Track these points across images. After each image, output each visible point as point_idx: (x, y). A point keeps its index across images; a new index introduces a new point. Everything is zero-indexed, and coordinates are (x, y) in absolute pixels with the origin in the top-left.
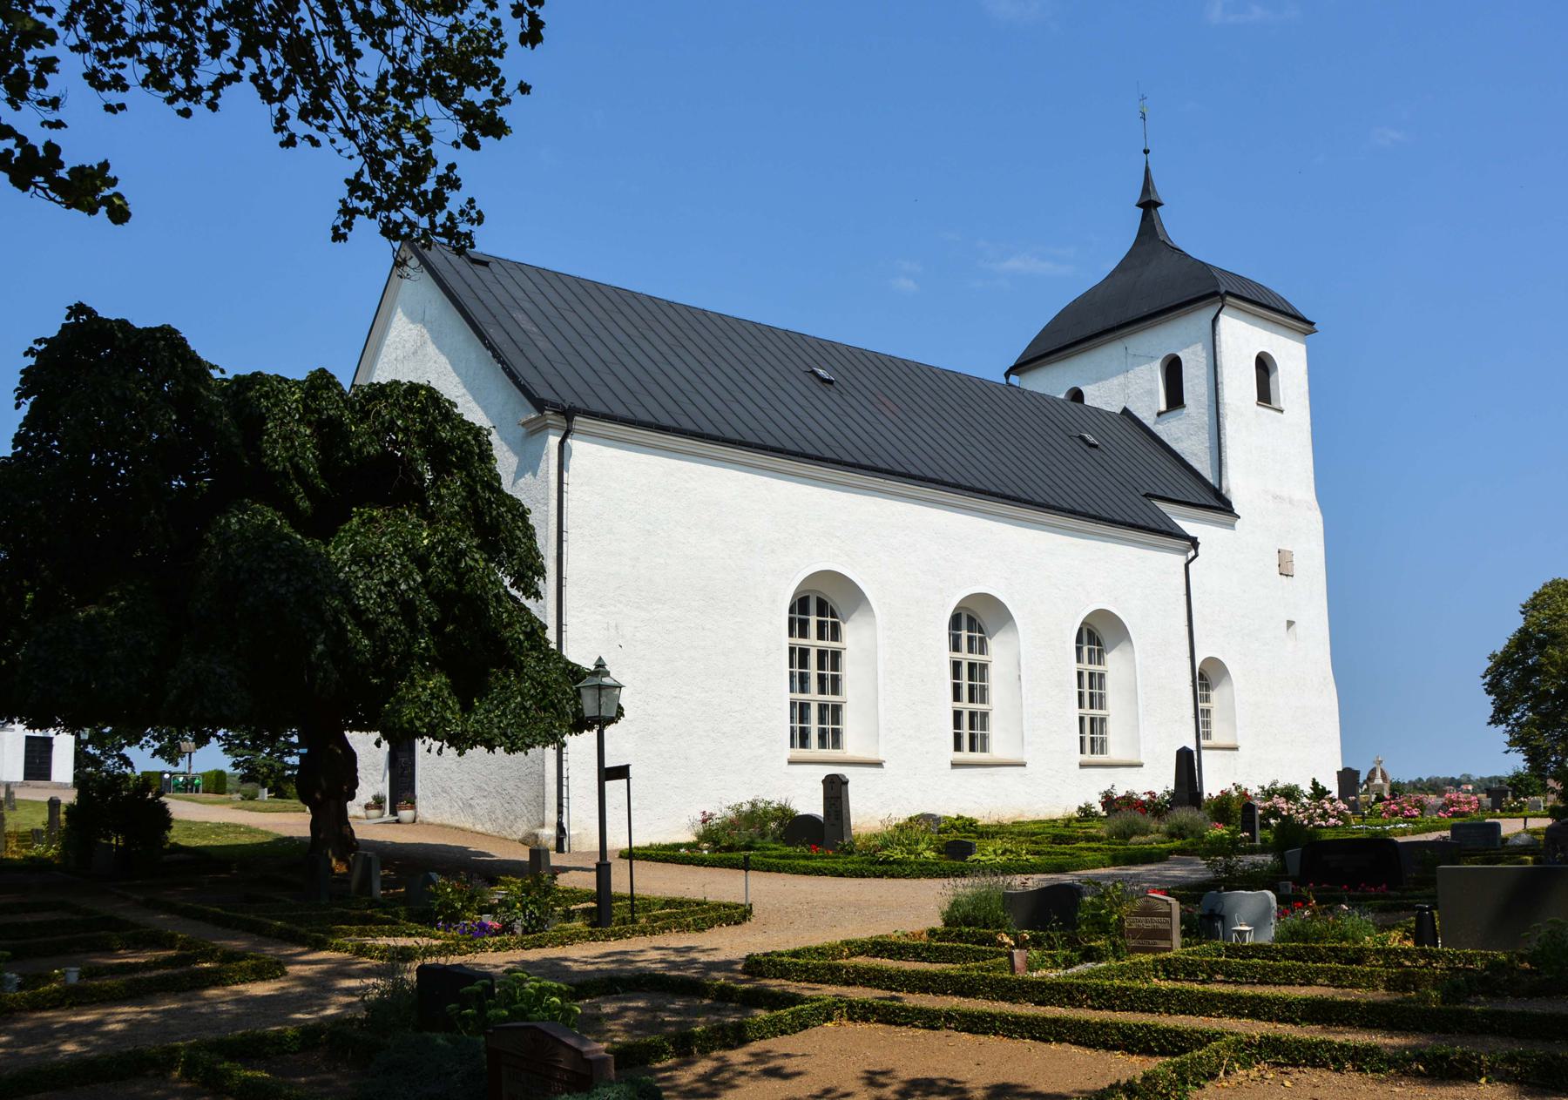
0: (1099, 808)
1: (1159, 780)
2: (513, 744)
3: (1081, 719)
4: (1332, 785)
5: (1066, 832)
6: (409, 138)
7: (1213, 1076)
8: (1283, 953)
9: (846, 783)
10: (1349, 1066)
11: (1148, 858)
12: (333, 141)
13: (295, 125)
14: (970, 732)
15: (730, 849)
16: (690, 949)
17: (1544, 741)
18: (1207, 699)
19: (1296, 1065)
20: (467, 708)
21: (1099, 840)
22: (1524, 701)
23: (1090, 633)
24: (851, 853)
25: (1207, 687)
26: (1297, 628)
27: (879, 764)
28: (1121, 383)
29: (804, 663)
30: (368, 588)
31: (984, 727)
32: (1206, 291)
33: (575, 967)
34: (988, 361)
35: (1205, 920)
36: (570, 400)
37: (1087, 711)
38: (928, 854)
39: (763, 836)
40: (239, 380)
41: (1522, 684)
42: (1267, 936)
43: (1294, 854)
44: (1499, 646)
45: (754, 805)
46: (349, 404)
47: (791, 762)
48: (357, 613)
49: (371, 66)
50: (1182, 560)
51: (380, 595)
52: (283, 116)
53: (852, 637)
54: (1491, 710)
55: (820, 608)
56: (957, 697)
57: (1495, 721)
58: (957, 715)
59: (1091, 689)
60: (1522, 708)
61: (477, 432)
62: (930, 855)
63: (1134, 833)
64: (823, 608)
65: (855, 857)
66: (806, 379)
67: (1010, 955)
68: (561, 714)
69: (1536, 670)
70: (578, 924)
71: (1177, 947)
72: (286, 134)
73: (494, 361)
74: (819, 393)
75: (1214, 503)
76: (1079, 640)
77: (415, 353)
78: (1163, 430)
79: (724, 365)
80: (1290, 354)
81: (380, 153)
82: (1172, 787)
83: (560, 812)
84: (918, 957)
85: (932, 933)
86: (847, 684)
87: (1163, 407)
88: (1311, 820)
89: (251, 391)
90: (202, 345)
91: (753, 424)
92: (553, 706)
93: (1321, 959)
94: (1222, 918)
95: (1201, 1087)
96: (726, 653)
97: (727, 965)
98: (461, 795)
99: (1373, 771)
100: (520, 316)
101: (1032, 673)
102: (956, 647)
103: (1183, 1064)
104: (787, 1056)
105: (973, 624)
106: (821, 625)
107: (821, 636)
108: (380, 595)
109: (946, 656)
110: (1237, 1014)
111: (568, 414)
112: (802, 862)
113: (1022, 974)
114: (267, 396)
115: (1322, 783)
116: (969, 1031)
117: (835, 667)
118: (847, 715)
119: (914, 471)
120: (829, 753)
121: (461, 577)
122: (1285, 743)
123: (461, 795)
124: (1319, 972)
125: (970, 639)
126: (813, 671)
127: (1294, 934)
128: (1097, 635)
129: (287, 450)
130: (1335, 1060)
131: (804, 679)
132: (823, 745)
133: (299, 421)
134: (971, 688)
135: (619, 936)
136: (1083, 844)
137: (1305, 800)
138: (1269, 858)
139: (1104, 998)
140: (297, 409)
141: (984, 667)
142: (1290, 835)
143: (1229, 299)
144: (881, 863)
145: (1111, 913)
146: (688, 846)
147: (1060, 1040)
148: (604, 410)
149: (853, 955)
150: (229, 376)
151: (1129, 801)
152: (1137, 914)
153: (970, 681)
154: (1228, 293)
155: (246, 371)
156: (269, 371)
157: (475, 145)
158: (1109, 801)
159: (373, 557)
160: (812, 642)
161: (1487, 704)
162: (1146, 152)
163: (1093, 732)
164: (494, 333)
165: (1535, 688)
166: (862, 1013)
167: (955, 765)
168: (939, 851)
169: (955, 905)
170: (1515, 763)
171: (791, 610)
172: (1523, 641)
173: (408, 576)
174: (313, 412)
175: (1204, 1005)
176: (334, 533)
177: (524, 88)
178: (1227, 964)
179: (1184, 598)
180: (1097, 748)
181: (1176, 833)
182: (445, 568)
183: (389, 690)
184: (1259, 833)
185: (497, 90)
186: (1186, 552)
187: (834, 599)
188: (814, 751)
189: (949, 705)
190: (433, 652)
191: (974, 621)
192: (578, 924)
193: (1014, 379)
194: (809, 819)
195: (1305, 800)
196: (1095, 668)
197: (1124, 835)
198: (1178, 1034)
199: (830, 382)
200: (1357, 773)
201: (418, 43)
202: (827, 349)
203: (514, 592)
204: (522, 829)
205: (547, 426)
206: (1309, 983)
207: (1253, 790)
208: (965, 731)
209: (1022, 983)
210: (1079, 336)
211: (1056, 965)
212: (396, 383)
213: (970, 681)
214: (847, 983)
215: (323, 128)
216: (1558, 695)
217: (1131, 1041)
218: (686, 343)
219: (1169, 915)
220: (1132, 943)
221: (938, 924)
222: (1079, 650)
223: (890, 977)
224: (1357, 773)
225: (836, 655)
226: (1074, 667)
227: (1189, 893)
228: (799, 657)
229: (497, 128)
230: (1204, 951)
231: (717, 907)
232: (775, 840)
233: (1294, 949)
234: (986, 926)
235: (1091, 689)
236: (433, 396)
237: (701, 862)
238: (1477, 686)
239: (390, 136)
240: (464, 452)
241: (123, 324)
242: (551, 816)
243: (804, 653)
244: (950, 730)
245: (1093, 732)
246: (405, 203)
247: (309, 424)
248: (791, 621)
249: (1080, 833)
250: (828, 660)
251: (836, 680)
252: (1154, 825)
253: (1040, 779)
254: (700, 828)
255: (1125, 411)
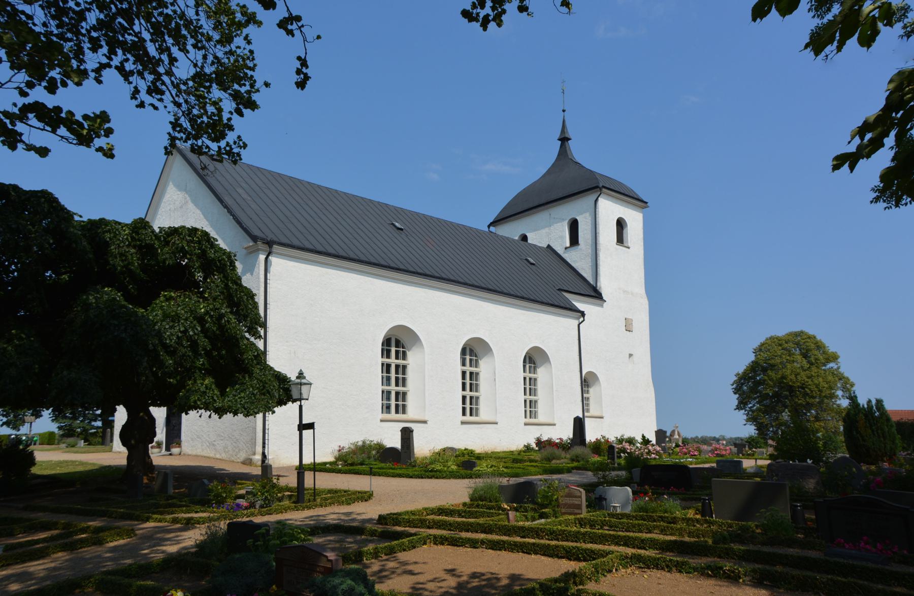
0: (534, 446)
1: (565, 432)
2: (248, 412)
3: (525, 401)
4: (652, 438)
5: (519, 457)
6: (211, 109)
7: (610, 571)
8: (636, 518)
9: (412, 431)
10: (674, 569)
11: (559, 471)
12: (165, 107)
13: (143, 96)
14: (470, 406)
15: (352, 465)
16: (351, 513)
17: (766, 420)
18: (588, 392)
19: (649, 568)
20: (223, 394)
21: (536, 461)
22: (755, 399)
23: (530, 358)
24: (415, 466)
25: (588, 386)
26: (635, 358)
27: (425, 422)
28: (547, 232)
29: (388, 371)
30: (172, 334)
31: (477, 404)
32: (592, 186)
33: (331, 522)
34: (479, 218)
35: (597, 502)
36: (270, 237)
37: (528, 397)
38: (453, 467)
39: (369, 458)
40: (91, 222)
41: (753, 390)
42: (628, 510)
43: (637, 471)
44: (741, 370)
45: (364, 442)
46: (157, 237)
47: (381, 421)
48: (165, 347)
49: (184, 70)
50: (576, 322)
51: (178, 337)
52: (136, 91)
53: (413, 359)
54: (736, 402)
55: (396, 344)
56: (464, 389)
57: (738, 408)
58: (464, 398)
59: (530, 386)
60: (753, 402)
61: (229, 255)
62: (454, 467)
63: (554, 458)
64: (398, 343)
65: (417, 468)
66: (390, 228)
67: (508, 514)
68: (272, 396)
69: (760, 383)
70: (286, 503)
71: (584, 514)
72: (139, 100)
73: (228, 215)
74: (396, 235)
75: (593, 294)
76: (525, 361)
77: (181, 207)
78: (567, 256)
79: (348, 220)
80: (634, 219)
81: (194, 115)
82: (571, 436)
83: (264, 447)
84: (460, 516)
85: (465, 504)
86: (410, 382)
87: (568, 245)
88: (642, 454)
89: (97, 227)
90: (68, 201)
91: (364, 251)
92: (268, 392)
93: (655, 521)
94: (606, 499)
95: (605, 576)
96: (361, 368)
97: (370, 521)
98: (205, 438)
99: (673, 432)
100: (240, 191)
101: (501, 376)
102: (464, 364)
103: (597, 564)
104: (416, 563)
105: (472, 353)
106: (397, 352)
107: (397, 358)
108: (178, 337)
109: (459, 368)
110: (618, 544)
111: (270, 244)
112: (391, 471)
113: (513, 523)
114: (109, 231)
115: (647, 436)
116: (493, 549)
117: (404, 373)
118: (409, 397)
119: (444, 276)
120: (400, 416)
121: (221, 327)
122: (628, 415)
123: (205, 438)
124: (655, 527)
125: (471, 360)
126: (393, 375)
127: (641, 509)
128: (533, 359)
129: (123, 261)
130: (668, 566)
131: (388, 379)
132: (397, 412)
133: (128, 246)
134: (471, 384)
135: (309, 508)
136: (528, 464)
137: (639, 445)
138: (624, 473)
139: (553, 535)
140: (127, 239)
141: (477, 374)
142: (634, 461)
143: (604, 190)
144: (431, 471)
145: (553, 495)
146: (330, 463)
147: (536, 553)
148: (312, 247)
149: (428, 515)
150: (85, 219)
151: (550, 443)
152: (566, 496)
153: (470, 381)
154: (604, 187)
155: (96, 217)
156: (109, 217)
157: (241, 114)
158: (539, 442)
159: (172, 315)
160: (393, 361)
161: (734, 399)
162: (564, 111)
163: (531, 407)
164: (227, 199)
165: (760, 392)
166: (440, 541)
167: (463, 423)
168: (458, 465)
169: (475, 490)
170: (750, 431)
171: (383, 345)
172: (754, 367)
173: (194, 328)
174: (136, 240)
175: (602, 539)
176: (150, 304)
177: (267, 85)
178: (610, 521)
179: (577, 342)
180: (533, 416)
181: (575, 459)
182: (215, 323)
183: (182, 385)
184: (617, 460)
185: (252, 86)
186: (578, 319)
187: (404, 339)
188: (393, 415)
189: (460, 393)
190: (207, 366)
191: (473, 351)
192: (286, 503)
193: (492, 229)
194: (393, 450)
195: (639, 445)
196: (532, 375)
197: (549, 460)
198: (592, 551)
199: (401, 229)
200: (665, 432)
201: (210, 58)
202: (399, 212)
203: (247, 335)
204: (242, 456)
205: (258, 250)
206: (650, 532)
207: (612, 438)
208: (468, 406)
209: (514, 527)
210: (526, 207)
211: (527, 519)
212: (184, 227)
213: (470, 381)
214: (429, 528)
215: (161, 100)
216: (773, 397)
217: (570, 555)
218: (328, 207)
219: (580, 497)
220: (563, 510)
221: (467, 500)
222: (524, 366)
223: (450, 524)
224: (665, 432)
225: (404, 367)
226: (522, 375)
227: (590, 488)
228: (387, 368)
229: (253, 105)
230: (597, 515)
231: (355, 493)
232: (375, 460)
233: (641, 516)
234: (491, 501)
235: (530, 386)
236: (206, 234)
237: (339, 471)
238: (729, 389)
239: (200, 108)
240: (220, 265)
241: (15, 187)
242: (259, 449)
243: (389, 366)
244: (461, 405)
245: (531, 407)
246: (202, 139)
247: (134, 247)
248: (383, 350)
249: (526, 458)
250: (401, 370)
251: (404, 380)
252: (563, 454)
253: (504, 431)
254: (337, 453)
255: (549, 246)
